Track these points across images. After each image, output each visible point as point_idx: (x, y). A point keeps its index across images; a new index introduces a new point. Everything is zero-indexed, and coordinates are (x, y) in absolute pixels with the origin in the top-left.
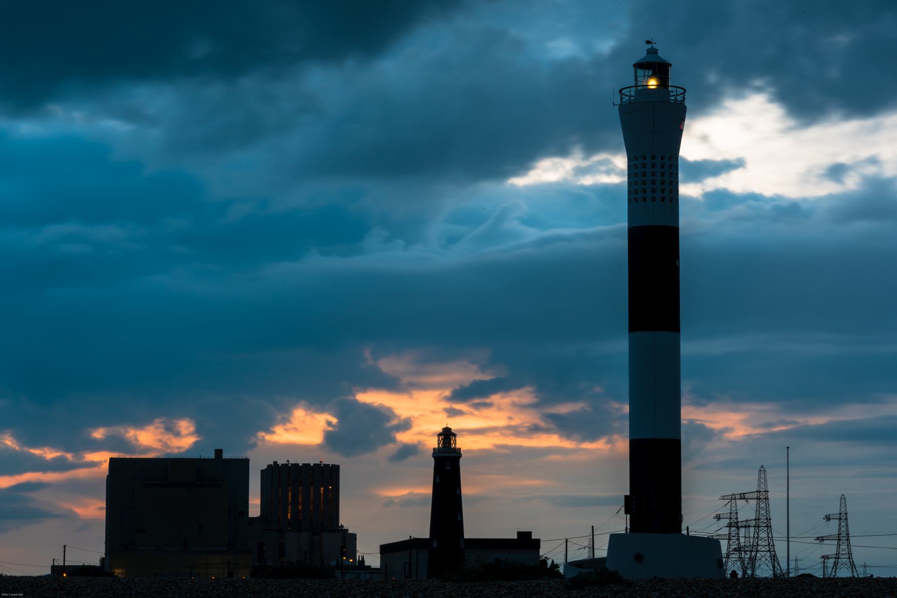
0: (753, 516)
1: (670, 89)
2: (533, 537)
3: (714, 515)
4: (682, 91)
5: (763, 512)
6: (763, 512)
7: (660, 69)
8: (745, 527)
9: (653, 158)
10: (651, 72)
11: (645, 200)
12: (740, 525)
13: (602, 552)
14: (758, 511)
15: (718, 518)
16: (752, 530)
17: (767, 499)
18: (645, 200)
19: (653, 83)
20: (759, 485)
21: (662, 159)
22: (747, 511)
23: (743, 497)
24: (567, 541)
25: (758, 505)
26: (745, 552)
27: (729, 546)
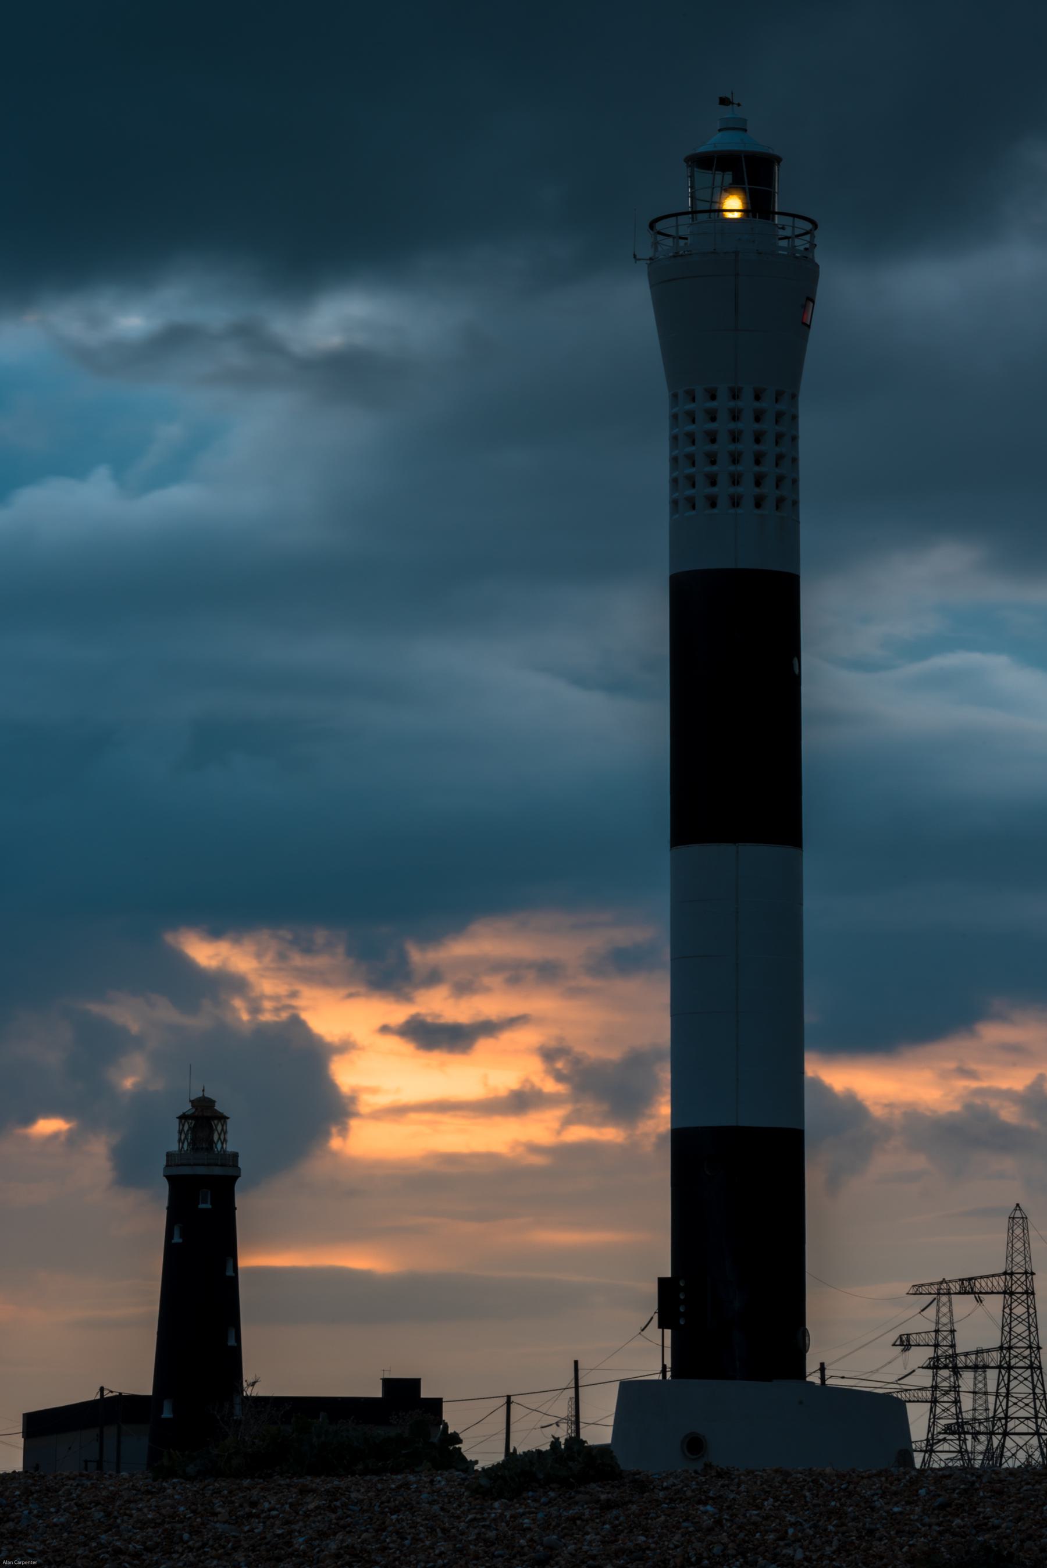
0: (993, 1339)
1: (777, 219)
2: (424, 1395)
3: (894, 1336)
4: (808, 226)
5: (1020, 1329)
6: (1020, 1329)
7: (754, 173)
8: (975, 1368)
9: (735, 395)
10: (729, 177)
11: (713, 505)
12: (961, 1361)
13: (599, 1432)
14: (1007, 1326)
15: (905, 1343)
16: (992, 1375)
17: (1030, 1293)
18: (713, 505)
19: (733, 204)
20: (1010, 1257)
21: (757, 398)
22: (978, 1325)
23: (968, 1287)
24: (509, 1402)
25: (1008, 1307)
26: (975, 1435)
27: (934, 1419)
